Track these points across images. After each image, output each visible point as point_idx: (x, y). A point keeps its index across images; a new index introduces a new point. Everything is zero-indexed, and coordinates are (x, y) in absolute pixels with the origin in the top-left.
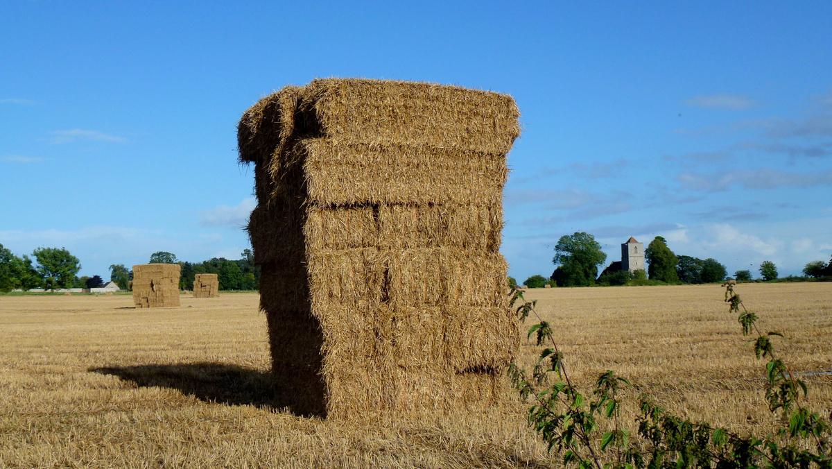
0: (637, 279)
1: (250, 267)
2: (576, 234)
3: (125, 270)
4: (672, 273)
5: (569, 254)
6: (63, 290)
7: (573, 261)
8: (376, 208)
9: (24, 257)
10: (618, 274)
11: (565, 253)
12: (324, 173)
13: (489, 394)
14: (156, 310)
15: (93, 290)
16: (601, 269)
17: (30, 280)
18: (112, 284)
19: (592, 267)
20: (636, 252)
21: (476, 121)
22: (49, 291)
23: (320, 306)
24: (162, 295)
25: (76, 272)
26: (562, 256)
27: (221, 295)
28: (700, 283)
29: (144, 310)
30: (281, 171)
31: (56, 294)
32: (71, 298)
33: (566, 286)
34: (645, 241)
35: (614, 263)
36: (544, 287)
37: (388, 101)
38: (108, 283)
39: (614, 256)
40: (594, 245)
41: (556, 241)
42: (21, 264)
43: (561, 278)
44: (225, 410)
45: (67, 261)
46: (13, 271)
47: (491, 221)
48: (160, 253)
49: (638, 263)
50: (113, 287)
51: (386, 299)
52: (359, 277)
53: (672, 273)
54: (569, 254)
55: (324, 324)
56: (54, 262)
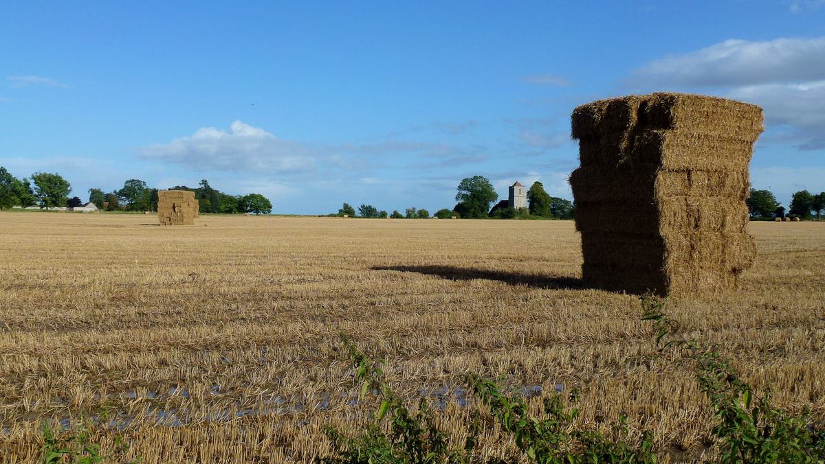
0: (521, 214)
1: (206, 195)
2: (475, 178)
3: (101, 193)
4: (547, 211)
5: (468, 193)
6: (56, 208)
7: (473, 199)
8: (689, 172)
9: (24, 180)
10: (506, 210)
11: (464, 192)
12: (671, 151)
13: (733, 285)
14: (177, 227)
15: (75, 209)
16: (492, 205)
17: (29, 199)
18: (91, 204)
19: (486, 204)
20: (520, 193)
21: (744, 121)
22: (45, 208)
23: (665, 231)
24: (182, 216)
25: (68, 194)
26: (463, 195)
27: (200, 216)
28: (566, 219)
29: (168, 227)
30: (630, 147)
31: (50, 211)
32: (60, 214)
33: (466, 218)
34: (528, 183)
35: (502, 201)
36: (451, 218)
37: (705, 109)
38: (87, 204)
39: (504, 196)
40: (489, 186)
41: (458, 183)
42: (21, 185)
43: (462, 211)
44: (585, 291)
45: (61, 184)
46: (14, 191)
47: (744, 182)
48: (133, 180)
49: (521, 202)
50: (92, 207)
51: (697, 226)
52: (684, 214)
53: (547, 211)
54: (468, 193)
55: (667, 241)
56: (49, 184)
